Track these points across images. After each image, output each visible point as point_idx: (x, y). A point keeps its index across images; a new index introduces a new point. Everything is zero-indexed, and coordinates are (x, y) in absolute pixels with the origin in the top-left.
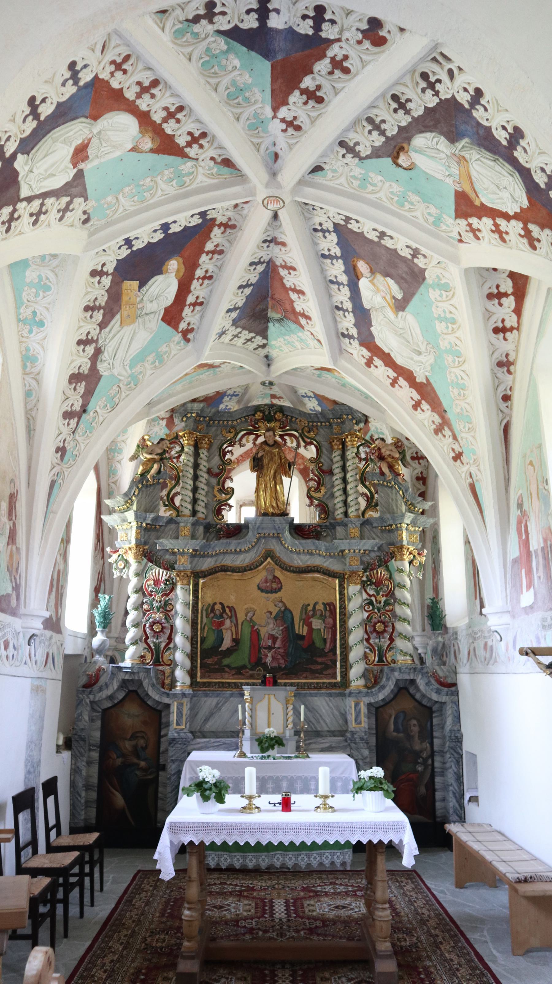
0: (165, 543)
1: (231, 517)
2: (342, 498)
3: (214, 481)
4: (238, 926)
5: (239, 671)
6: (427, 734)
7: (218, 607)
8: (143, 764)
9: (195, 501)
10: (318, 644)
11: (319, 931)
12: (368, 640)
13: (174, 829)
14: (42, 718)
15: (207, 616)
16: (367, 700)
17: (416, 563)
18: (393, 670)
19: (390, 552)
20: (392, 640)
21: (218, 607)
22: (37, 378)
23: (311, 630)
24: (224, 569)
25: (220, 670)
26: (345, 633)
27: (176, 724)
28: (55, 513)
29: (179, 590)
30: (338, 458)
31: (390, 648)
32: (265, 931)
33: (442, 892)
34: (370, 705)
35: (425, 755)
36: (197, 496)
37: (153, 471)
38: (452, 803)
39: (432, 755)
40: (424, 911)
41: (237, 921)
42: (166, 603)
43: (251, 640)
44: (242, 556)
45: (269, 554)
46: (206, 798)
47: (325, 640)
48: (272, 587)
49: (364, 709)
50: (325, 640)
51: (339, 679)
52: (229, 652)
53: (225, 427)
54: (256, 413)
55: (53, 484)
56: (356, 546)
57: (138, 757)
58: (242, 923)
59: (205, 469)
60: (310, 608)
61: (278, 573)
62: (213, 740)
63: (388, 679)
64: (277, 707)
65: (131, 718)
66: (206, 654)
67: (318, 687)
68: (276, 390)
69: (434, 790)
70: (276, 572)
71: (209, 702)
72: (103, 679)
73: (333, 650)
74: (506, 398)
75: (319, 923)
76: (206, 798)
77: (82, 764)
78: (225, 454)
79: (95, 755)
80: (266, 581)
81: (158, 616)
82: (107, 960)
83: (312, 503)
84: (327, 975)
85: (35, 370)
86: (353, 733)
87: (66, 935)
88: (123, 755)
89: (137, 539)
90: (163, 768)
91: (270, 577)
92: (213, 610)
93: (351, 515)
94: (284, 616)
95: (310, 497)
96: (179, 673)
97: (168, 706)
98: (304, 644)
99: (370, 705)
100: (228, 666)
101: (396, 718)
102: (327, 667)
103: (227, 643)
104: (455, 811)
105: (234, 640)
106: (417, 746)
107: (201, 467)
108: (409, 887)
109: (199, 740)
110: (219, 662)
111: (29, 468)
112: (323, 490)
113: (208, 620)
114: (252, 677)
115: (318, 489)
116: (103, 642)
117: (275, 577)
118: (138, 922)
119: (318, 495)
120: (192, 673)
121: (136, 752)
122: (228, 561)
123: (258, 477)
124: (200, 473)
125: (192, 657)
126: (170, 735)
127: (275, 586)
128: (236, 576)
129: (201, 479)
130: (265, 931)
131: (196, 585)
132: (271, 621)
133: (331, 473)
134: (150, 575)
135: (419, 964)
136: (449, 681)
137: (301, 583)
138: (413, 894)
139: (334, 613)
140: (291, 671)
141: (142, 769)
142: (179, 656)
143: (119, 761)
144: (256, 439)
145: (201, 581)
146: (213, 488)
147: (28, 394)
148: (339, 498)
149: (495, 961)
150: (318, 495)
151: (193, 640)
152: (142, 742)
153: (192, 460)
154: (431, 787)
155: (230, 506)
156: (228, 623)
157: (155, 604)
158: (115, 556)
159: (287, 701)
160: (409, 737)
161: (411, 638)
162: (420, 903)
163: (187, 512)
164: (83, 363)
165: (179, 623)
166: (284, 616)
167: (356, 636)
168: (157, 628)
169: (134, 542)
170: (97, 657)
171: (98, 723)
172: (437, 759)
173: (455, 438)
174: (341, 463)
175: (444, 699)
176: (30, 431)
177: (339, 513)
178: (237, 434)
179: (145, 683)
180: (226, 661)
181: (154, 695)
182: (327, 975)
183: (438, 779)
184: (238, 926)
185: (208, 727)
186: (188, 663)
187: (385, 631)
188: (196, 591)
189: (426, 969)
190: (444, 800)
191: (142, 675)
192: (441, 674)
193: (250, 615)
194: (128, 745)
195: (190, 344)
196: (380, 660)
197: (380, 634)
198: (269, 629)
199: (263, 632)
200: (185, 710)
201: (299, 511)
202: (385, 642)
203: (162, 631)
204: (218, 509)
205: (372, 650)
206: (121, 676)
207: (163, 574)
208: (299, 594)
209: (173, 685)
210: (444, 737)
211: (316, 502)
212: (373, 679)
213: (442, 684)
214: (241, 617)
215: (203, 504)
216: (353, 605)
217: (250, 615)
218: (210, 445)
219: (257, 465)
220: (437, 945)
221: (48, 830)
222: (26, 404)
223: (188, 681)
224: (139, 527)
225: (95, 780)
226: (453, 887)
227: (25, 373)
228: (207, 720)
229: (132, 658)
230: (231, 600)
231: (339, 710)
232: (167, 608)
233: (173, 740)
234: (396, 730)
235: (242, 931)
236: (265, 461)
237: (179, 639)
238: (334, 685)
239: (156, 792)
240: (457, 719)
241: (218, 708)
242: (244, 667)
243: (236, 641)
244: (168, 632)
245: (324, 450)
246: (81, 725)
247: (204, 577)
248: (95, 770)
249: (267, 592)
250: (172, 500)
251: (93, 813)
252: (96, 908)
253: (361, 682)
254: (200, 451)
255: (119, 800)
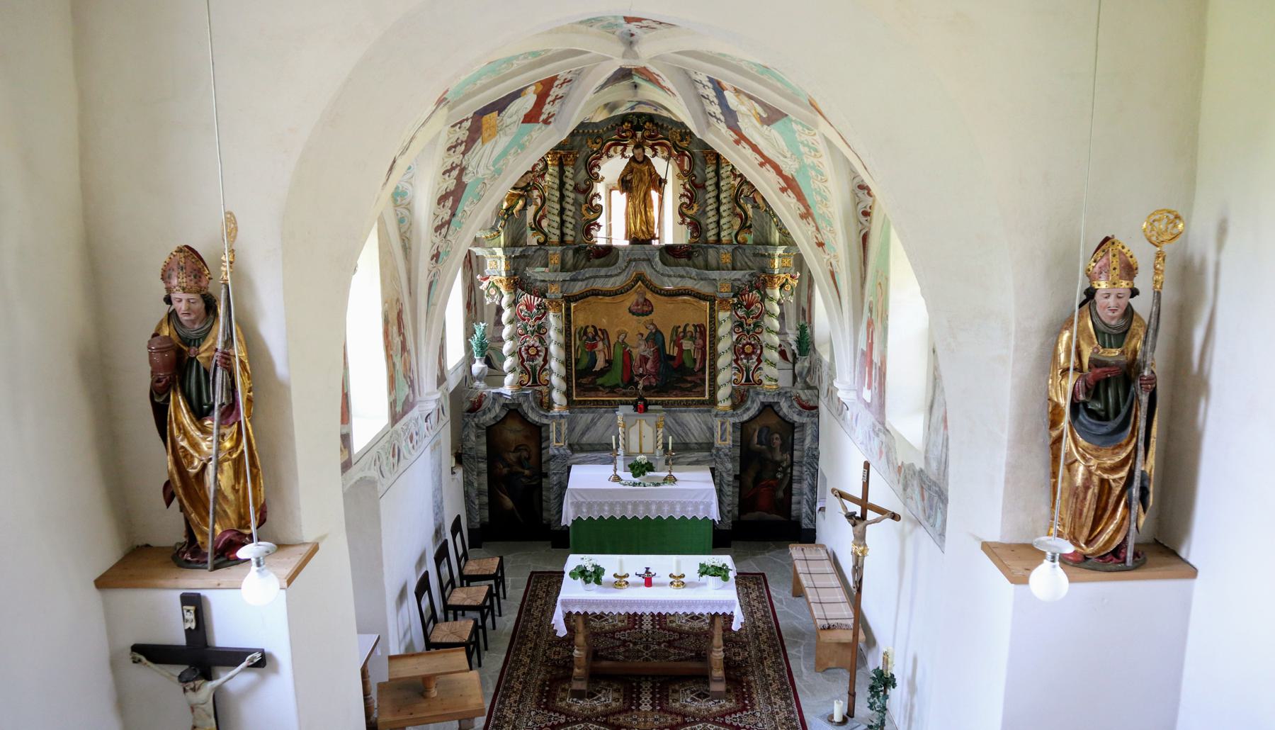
0: (537, 273)
1: (600, 238)
2: (715, 219)
3: (581, 198)
4: (613, 638)
5: (612, 390)
6: (788, 447)
7: (590, 330)
8: (527, 472)
9: (563, 222)
10: (688, 364)
11: (676, 644)
12: (736, 361)
13: (564, 603)
14: (440, 465)
15: (580, 339)
16: (732, 420)
17: (788, 288)
18: (758, 394)
19: (762, 280)
20: (759, 361)
21: (590, 330)
22: (409, 207)
23: (681, 350)
24: (596, 293)
25: (595, 389)
26: (715, 356)
27: (555, 445)
28: (435, 305)
29: (551, 317)
30: (713, 174)
31: (757, 368)
32: (635, 644)
33: (780, 601)
34: (734, 425)
35: (785, 465)
36: (565, 217)
37: (518, 207)
38: (805, 509)
39: (791, 465)
40: (760, 624)
41: (614, 633)
42: (540, 327)
43: (624, 361)
44: (612, 280)
45: (640, 277)
46: (587, 582)
47: (695, 360)
48: (643, 309)
49: (729, 429)
50: (695, 360)
51: (707, 397)
52: (603, 372)
53: (590, 135)
54: (623, 123)
55: (431, 284)
56: (724, 280)
57: (523, 467)
58: (618, 635)
59: (571, 188)
60: (681, 330)
61: (649, 296)
62: (589, 455)
63: (753, 402)
64: (648, 431)
65: (513, 433)
66: (580, 374)
67: (687, 404)
68: (648, 52)
69: (791, 495)
70: (645, 294)
71: (585, 418)
72: (485, 404)
73: (703, 370)
74: (866, 214)
75: (676, 636)
76: (587, 582)
77: (474, 478)
78: (591, 169)
79: (484, 466)
80: (637, 304)
81: (532, 341)
82: (520, 673)
83: (683, 222)
84: (677, 687)
85: (405, 202)
86: (718, 450)
87: (486, 649)
88: (509, 465)
89: (507, 271)
90: (546, 475)
91: (641, 300)
92: (585, 333)
93: (724, 240)
94: (655, 338)
95: (682, 214)
96: (556, 396)
97: (548, 425)
98: (674, 364)
99: (734, 425)
100: (602, 385)
101: (760, 432)
102: (696, 385)
103: (600, 364)
104: (807, 516)
105: (607, 361)
106: (778, 457)
107: (567, 186)
108: (754, 595)
109: (577, 455)
110: (593, 382)
111: (409, 280)
112: (696, 207)
113: (581, 343)
114: (624, 395)
115: (690, 207)
116: (483, 369)
117: (646, 300)
118: (538, 634)
119: (690, 212)
120: (568, 394)
121: (520, 462)
122: (599, 284)
123: (628, 198)
124: (567, 193)
125: (567, 379)
126: (551, 452)
127: (646, 309)
128: (607, 299)
129: (568, 199)
130: (635, 644)
131: (568, 309)
132: (643, 343)
133: (704, 187)
134: (522, 300)
135: (744, 678)
136: (811, 404)
137: (671, 306)
138: (756, 603)
139: (705, 334)
140: (662, 389)
141: (526, 477)
142: (555, 380)
143: (505, 471)
144: (624, 150)
145: (573, 305)
146: (581, 205)
147: (401, 221)
148: (712, 219)
149: (800, 677)
150: (690, 212)
151: (567, 363)
152: (525, 454)
153: (557, 181)
154: (789, 492)
155: (599, 226)
156: (600, 345)
157: (529, 329)
158: (486, 283)
159: (657, 426)
160: (771, 449)
161: (774, 375)
162: (758, 615)
163: (555, 239)
164: (450, 183)
165: (553, 348)
166: (655, 338)
167: (724, 360)
168: (532, 352)
169: (504, 274)
170: (477, 383)
171: (484, 439)
172: (796, 468)
173: (817, 229)
174: (714, 180)
175: (805, 420)
176: (406, 249)
177: (711, 235)
178: (604, 144)
179: (525, 406)
180: (599, 381)
181: (533, 417)
182: (677, 687)
183: (795, 486)
184: (613, 638)
185: (585, 440)
186: (564, 386)
187: (753, 353)
188: (568, 315)
189: (748, 683)
190: (799, 503)
191: (521, 399)
192: (804, 397)
193: (622, 337)
194: (512, 457)
195: (551, 126)
196: (748, 380)
197: (748, 356)
198: (640, 349)
199: (636, 353)
200: (564, 429)
201: (670, 232)
202: (753, 362)
203: (537, 354)
204: (588, 228)
205: (740, 370)
206: (502, 401)
207: (536, 301)
208: (668, 316)
209: (550, 405)
210: (803, 450)
211: (688, 220)
212: (739, 399)
213: (803, 407)
214: (613, 340)
215: (571, 226)
216: (723, 330)
217: (622, 337)
218: (576, 159)
219: (625, 184)
220: (761, 660)
221: (459, 561)
222: (399, 229)
223: (564, 402)
224: (508, 259)
225: (485, 487)
226: (790, 596)
227: (396, 206)
228: (583, 434)
229: (511, 385)
230: (603, 323)
231: (706, 425)
232: (540, 332)
233: (554, 456)
234: (760, 442)
235: (618, 643)
236: (635, 182)
237: (554, 364)
238: (703, 403)
239: (541, 495)
240: (816, 438)
241: (593, 423)
242: (617, 386)
243: (609, 362)
244: (542, 354)
245: (698, 162)
246: (469, 444)
247: (576, 301)
248: (484, 478)
249: (638, 315)
250: (539, 222)
251: (486, 513)
252: (504, 618)
253: (728, 403)
254: (566, 168)
255: (509, 503)
